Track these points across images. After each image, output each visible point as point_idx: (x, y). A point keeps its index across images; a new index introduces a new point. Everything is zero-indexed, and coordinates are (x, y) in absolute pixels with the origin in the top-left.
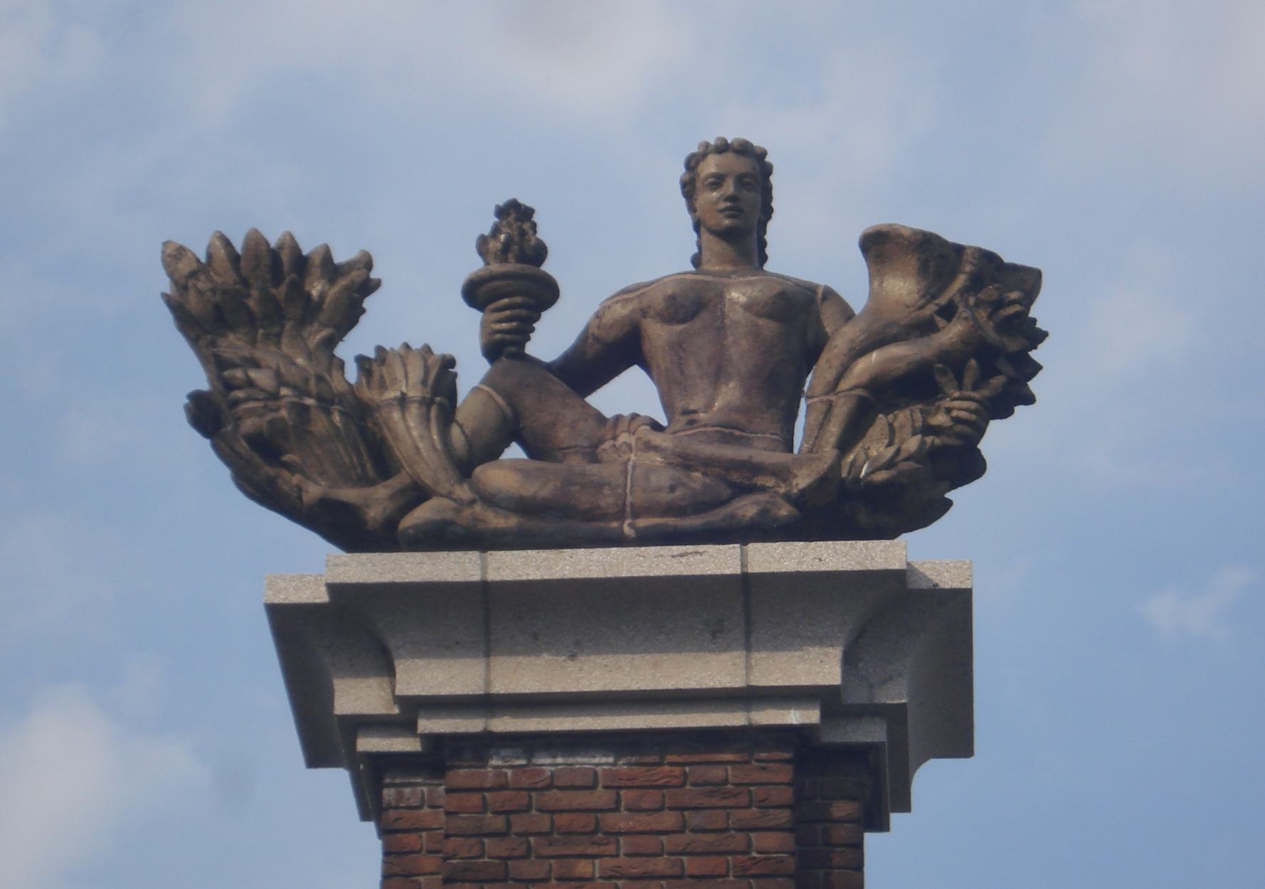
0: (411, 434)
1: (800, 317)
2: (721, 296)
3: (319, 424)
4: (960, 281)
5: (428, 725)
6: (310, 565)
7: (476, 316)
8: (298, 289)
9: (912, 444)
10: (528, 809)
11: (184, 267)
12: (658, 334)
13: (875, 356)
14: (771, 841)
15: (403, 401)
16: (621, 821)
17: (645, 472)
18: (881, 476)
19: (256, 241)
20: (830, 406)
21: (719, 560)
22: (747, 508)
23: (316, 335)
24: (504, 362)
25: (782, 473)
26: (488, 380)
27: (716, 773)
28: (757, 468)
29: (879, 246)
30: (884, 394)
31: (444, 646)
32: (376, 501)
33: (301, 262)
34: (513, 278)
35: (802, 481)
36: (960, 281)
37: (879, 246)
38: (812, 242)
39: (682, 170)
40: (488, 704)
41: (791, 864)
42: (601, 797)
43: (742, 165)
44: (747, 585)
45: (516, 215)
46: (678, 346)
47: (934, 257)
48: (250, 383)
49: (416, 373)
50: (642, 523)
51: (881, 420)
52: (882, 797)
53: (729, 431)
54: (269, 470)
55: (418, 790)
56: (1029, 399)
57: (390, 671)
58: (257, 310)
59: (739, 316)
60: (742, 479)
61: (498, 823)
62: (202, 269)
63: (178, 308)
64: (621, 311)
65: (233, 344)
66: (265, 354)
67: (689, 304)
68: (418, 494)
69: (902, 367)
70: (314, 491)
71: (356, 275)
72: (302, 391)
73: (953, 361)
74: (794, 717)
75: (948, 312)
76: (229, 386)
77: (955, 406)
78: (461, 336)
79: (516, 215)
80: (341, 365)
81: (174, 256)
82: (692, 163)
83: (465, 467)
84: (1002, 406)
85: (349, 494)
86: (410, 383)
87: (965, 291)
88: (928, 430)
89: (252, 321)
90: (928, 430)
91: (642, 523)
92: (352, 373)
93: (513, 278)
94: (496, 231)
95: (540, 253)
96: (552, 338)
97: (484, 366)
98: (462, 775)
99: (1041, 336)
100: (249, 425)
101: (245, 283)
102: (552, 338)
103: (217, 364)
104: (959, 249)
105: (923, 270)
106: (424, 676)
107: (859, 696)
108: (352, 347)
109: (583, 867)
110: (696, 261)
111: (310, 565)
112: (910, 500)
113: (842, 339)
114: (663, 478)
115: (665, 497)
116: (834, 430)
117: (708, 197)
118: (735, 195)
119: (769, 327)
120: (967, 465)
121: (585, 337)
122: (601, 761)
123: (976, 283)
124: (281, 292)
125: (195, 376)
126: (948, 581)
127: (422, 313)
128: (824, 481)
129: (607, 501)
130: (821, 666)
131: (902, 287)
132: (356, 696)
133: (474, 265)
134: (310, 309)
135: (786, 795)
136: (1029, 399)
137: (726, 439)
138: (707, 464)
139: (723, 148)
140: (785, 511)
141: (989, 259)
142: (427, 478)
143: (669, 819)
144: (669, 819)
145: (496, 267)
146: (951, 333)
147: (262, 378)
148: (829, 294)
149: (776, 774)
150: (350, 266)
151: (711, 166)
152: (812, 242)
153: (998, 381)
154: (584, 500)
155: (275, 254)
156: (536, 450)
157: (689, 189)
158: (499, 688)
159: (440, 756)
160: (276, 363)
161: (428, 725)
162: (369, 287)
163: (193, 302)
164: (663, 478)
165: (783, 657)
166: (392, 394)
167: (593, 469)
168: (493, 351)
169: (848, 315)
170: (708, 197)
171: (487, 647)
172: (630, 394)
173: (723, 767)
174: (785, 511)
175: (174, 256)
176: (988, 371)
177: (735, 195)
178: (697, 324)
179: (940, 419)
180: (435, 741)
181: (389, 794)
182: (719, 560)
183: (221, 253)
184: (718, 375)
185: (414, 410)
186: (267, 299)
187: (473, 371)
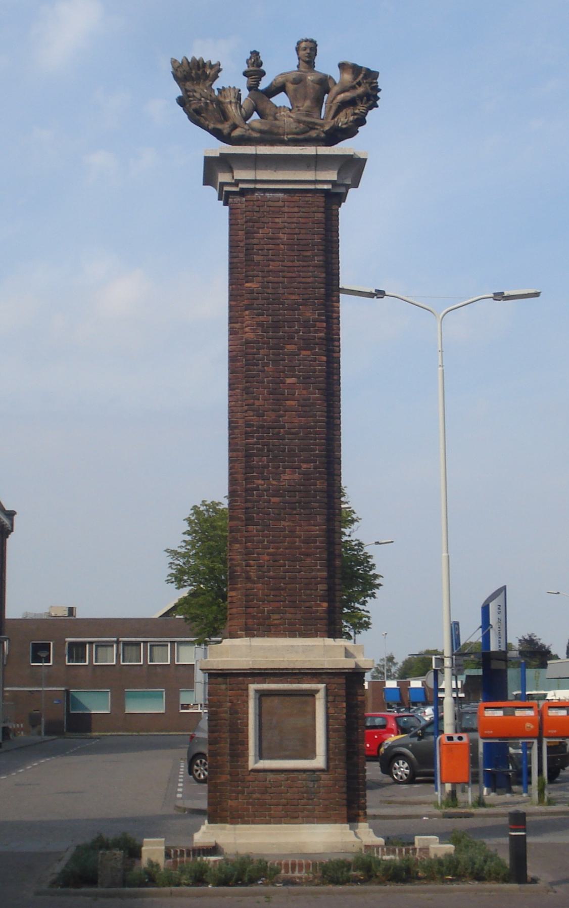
0: (232, 110)
1: (324, 84)
2: (306, 78)
3: (210, 108)
4: (362, 76)
5: (241, 186)
6: (218, 148)
7: (246, 79)
8: (204, 72)
9: (351, 118)
10: (263, 206)
11: (177, 65)
12: (290, 87)
13: (342, 95)
14: (320, 215)
15: (231, 102)
16: (286, 209)
17: (288, 122)
18: (344, 126)
19: (194, 59)
20: (331, 107)
21: (310, 150)
22: (313, 134)
23: (208, 83)
24: (253, 91)
25: (322, 126)
26: (249, 96)
27: (307, 199)
28: (316, 124)
29: (342, 66)
30: (344, 105)
31: (246, 168)
32: (225, 127)
33: (204, 65)
34: (255, 70)
35: (327, 128)
36: (362, 76)
37: (342, 66)
38: (327, 64)
39: (296, 45)
40: (255, 181)
41: (324, 220)
42: (280, 204)
43: (311, 45)
44: (317, 157)
45: (255, 54)
46: (295, 90)
47: (356, 70)
48: (194, 96)
49: (233, 94)
50: (289, 136)
51: (344, 111)
52: (340, 198)
53: (308, 114)
54: (198, 117)
55: (237, 199)
56: (377, 106)
57: (232, 172)
58: (193, 75)
59: (309, 86)
60: (312, 126)
61: (257, 209)
62: (181, 65)
63: (176, 78)
64: (280, 80)
65: (189, 85)
66: (196, 88)
67: (299, 81)
68: (235, 127)
69: (348, 98)
70: (211, 126)
71: (217, 68)
72: (207, 99)
73: (361, 97)
74: (325, 187)
75: (359, 84)
76: (189, 97)
77: (360, 109)
78: (242, 84)
79: (255, 54)
80: (214, 91)
81: (174, 62)
82: (299, 43)
83: (246, 118)
84: (370, 108)
85: (219, 126)
86: (231, 98)
87: (363, 78)
88: (354, 114)
89: (193, 79)
90: (354, 114)
91: (289, 136)
92: (216, 93)
93: (255, 70)
94: (251, 58)
95: (261, 64)
96: (264, 84)
97: (247, 92)
98: (249, 197)
99: (380, 90)
100: (194, 106)
101: (191, 69)
102: (264, 84)
103: (185, 91)
104: (361, 67)
105: (353, 73)
106: (241, 174)
107: (340, 182)
108: (217, 85)
109: (277, 220)
110: (298, 67)
111: (218, 148)
112: (349, 132)
113: (335, 90)
114: (294, 125)
115: (294, 130)
116: (332, 113)
117: (302, 53)
118: (308, 52)
119: (317, 87)
120: (361, 121)
121: (272, 84)
122: (281, 195)
123: (365, 77)
124: (200, 72)
125: (179, 92)
126: (362, 157)
127: (232, 79)
128: (331, 128)
129: (281, 131)
130: (332, 176)
131: (348, 77)
132: (223, 177)
133: (245, 67)
134: (207, 77)
135: (323, 204)
136: (377, 106)
137: (307, 115)
138: (304, 122)
139: (307, 41)
140: (323, 135)
141: (368, 70)
142: (237, 123)
143: (296, 210)
144: (296, 210)
145: (251, 68)
146: (360, 90)
147: (197, 95)
148: (330, 77)
149: (321, 199)
150: (215, 65)
151: (303, 45)
152: (327, 64)
153: (371, 102)
154: (276, 131)
155: (198, 62)
156: (261, 115)
157: (297, 50)
158: (258, 178)
159: (243, 192)
160: (200, 90)
161: (241, 186)
162: (220, 70)
163: (179, 74)
164: (294, 125)
165: (324, 173)
166: (228, 100)
167: (277, 122)
168: (250, 89)
169: (335, 84)
170: (302, 53)
171: (255, 168)
172: (281, 100)
173: (309, 198)
174: (323, 135)
175: (174, 62)
176: (368, 100)
177: (308, 52)
178: (300, 85)
179: (357, 111)
180: (242, 189)
181: (230, 200)
182: (310, 150)
183: (185, 62)
184: (305, 98)
185: (233, 105)
186: (196, 74)
187: (245, 93)
